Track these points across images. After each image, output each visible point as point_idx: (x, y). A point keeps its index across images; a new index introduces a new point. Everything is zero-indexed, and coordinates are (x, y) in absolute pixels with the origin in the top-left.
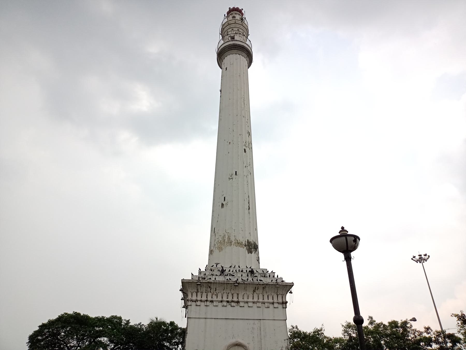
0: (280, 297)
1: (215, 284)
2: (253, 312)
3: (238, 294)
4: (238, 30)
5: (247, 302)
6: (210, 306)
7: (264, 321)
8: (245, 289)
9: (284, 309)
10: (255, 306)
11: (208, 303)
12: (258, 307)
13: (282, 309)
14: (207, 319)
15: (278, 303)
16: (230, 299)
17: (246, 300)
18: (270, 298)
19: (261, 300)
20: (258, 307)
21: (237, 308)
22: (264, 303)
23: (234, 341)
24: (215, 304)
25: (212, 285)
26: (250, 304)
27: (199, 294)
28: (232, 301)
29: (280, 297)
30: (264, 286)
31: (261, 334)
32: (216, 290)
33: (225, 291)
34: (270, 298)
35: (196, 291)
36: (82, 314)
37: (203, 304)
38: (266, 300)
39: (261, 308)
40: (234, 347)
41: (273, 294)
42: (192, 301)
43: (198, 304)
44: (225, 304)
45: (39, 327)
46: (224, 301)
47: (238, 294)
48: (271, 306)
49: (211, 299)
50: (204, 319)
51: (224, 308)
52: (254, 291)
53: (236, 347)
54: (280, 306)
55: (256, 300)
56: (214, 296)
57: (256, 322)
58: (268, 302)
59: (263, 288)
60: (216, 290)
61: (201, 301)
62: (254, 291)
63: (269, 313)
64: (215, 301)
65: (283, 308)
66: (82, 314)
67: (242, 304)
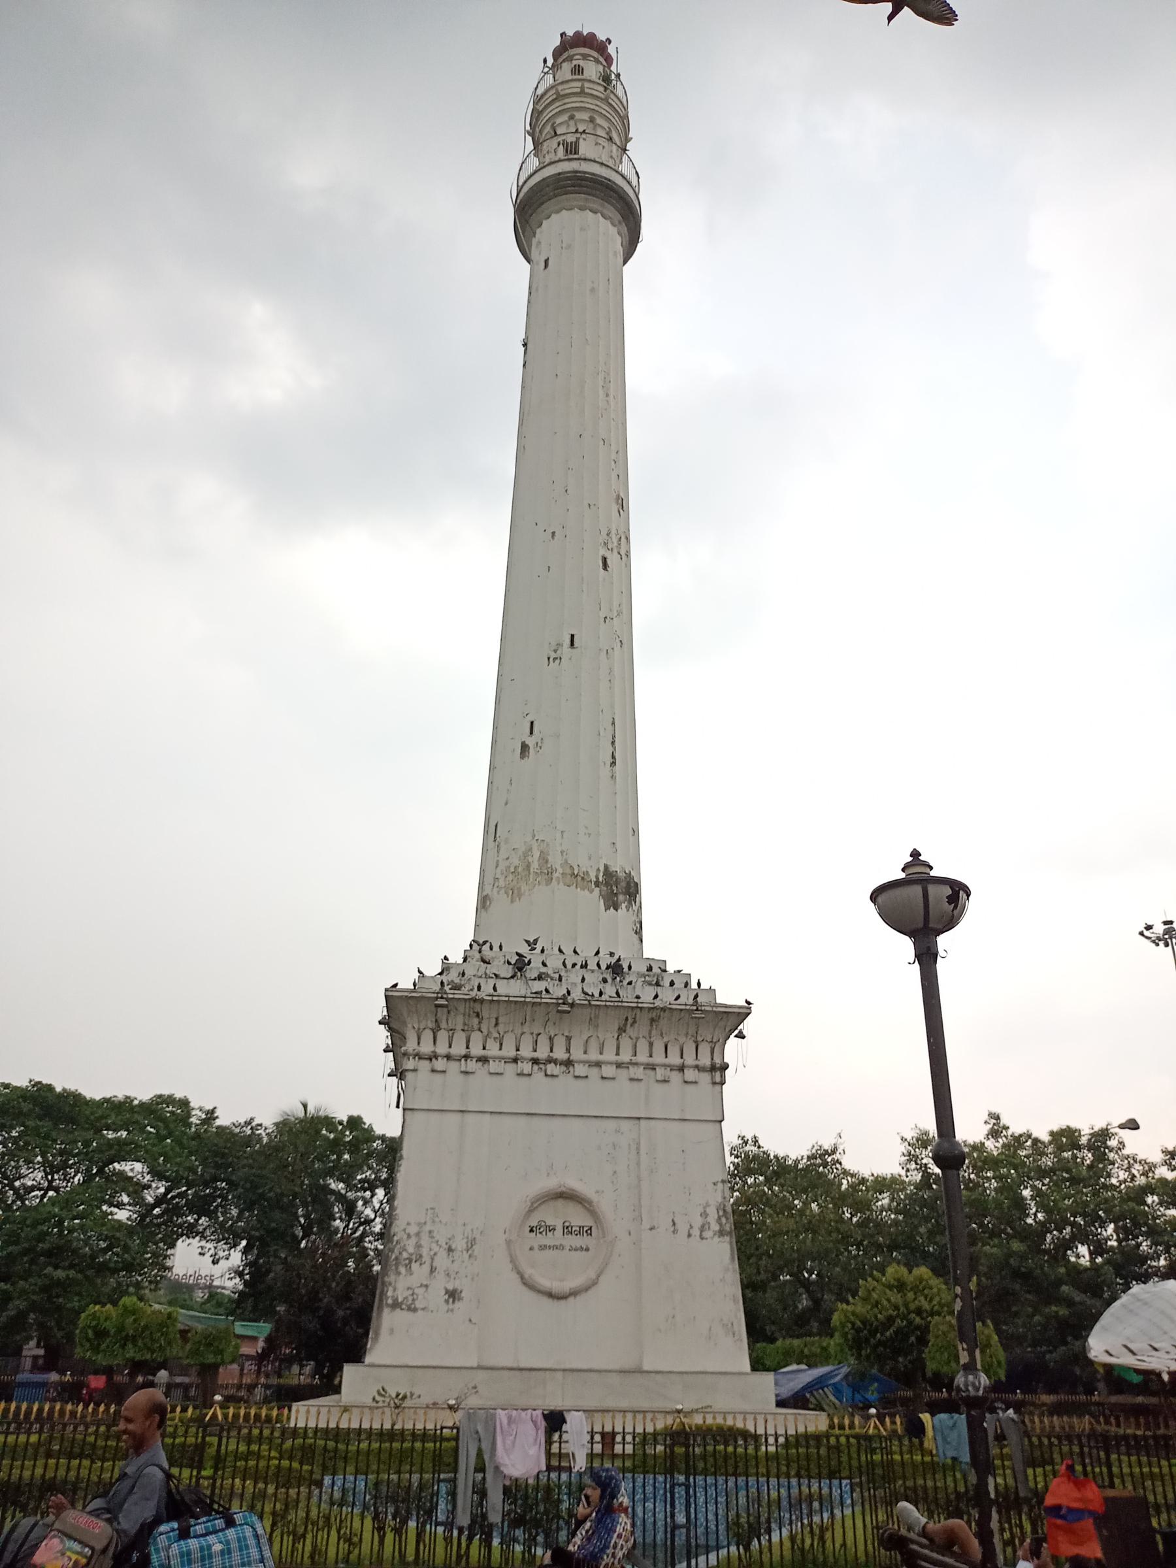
0: (705, 1049)
1: (495, 1006)
2: (621, 1095)
3: (569, 1039)
4: (592, 120)
5: (598, 1064)
8: (593, 1022)
9: (718, 1087)
10: (623, 1074)
11: (472, 1065)
12: (631, 1079)
14: (467, 1116)
16: (542, 1053)
17: (594, 1056)
18: (674, 1052)
20: (631, 1079)
21: (565, 1081)
24: (493, 1066)
25: (486, 1006)
26: (608, 1071)
27: (443, 1036)
32: (497, 1024)
34: (674, 1052)
35: (431, 1025)
36: (58, 1089)
38: (659, 1058)
41: (682, 1039)
42: (419, 1056)
44: (527, 1067)
47: (569, 1039)
48: (675, 1077)
50: (460, 1114)
52: (622, 1030)
53: (560, 1203)
54: (705, 1078)
55: (625, 1057)
57: (625, 1125)
58: (665, 1066)
59: (652, 1020)
61: (448, 1057)
62: (622, 1030)
63: (669, 1097)
65: (714, 1083)
66: (58, 1089)
67: (580, 1070)
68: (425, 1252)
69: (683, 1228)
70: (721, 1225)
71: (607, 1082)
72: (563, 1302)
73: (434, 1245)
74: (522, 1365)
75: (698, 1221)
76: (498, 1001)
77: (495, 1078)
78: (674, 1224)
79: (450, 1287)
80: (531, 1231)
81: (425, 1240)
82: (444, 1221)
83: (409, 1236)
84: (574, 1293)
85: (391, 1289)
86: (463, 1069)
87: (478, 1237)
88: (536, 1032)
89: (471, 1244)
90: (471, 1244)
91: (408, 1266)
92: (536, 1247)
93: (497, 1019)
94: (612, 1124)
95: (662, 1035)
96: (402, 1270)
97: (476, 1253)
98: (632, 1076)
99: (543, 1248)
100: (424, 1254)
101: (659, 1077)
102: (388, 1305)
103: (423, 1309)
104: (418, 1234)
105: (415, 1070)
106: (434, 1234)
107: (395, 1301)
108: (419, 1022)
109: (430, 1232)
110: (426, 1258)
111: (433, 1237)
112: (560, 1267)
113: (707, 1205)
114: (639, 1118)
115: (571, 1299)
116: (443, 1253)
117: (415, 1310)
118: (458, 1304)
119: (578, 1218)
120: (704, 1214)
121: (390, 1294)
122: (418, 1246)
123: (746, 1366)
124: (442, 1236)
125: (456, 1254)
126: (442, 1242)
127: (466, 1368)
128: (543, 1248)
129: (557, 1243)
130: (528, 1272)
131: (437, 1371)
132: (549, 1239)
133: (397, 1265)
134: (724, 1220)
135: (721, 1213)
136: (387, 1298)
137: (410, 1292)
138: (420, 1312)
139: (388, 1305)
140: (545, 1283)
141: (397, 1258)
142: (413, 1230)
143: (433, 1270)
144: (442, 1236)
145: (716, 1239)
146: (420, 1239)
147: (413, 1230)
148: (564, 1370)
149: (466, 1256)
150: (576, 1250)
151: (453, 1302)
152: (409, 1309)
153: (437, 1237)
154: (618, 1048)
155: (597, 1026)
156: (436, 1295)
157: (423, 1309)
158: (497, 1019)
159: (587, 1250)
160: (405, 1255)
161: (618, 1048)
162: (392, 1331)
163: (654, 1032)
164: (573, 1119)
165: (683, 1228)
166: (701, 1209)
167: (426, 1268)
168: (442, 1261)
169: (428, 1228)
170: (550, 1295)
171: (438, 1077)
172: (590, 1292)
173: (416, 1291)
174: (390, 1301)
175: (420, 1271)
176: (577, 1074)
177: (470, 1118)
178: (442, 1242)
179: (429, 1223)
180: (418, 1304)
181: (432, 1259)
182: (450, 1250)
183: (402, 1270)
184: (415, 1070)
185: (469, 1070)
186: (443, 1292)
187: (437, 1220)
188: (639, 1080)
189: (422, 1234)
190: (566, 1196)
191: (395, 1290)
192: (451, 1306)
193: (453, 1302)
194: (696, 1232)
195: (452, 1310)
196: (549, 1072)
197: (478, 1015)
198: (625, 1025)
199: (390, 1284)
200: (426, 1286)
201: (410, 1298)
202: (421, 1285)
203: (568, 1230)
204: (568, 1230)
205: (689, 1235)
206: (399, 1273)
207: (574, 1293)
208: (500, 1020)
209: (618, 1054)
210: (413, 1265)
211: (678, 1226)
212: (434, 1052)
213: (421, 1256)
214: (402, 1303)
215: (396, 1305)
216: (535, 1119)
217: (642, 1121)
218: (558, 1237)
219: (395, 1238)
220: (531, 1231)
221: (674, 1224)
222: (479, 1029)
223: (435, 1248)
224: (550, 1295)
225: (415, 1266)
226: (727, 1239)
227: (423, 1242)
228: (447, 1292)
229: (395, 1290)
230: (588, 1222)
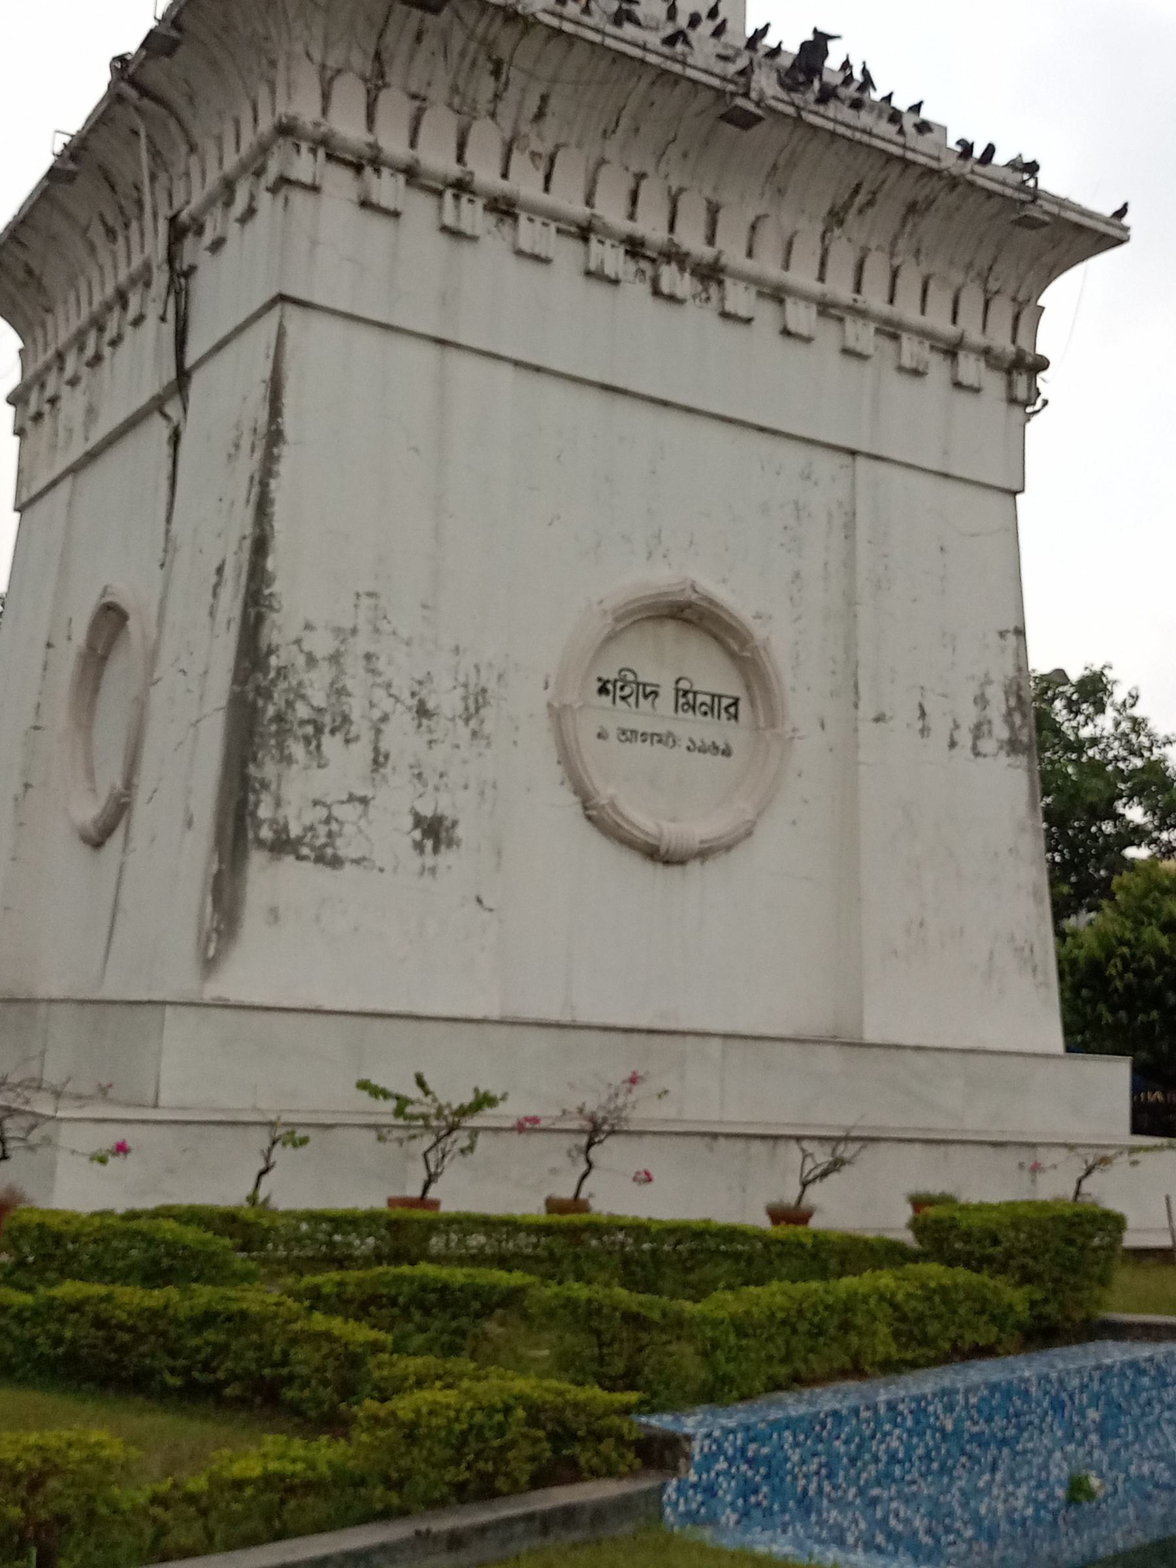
0: (1002, 311)
1: (556, 49)
2: (811, 383)
3: (713, 211)
6: (487, 241)
7: (882, 469)
8: (777, 180)
9: (1017, 412)
10: (828, 335)
12: (847, 352)
13: (1004, 405)
14: (452, 354)
15: (986, 353)
16: (651, 226)
17: (768, 266)
18: (940, 302)
19: (874, 298)
20: (847, 352)
21: (696, 318)
22: (891, 330)
23: (660, 578)
24: (529, 234)
25: (534, 42)
26: (801, 316)
27: (394, 106)
28: (674, 255)
29: (1002, 311)
30: (921, 193)
31: (849, 563)
32: (540, 115)
33: (611, 150)
34: (940, 302)
35: (361, 62)
37: (419, 209)
39: (868, 369)
40: (649, 627)
41: (957, 277)
43: (386, 202)
44: (613, 259)
45: (1042, 309)
46: (607, 233)
47: (713, 211)
49: (501, 186)
50: (432, 350)
51: (599, 291)
52: (836, 217)
53: (670, 629)
54: (994, 383)
55: (840, 288)
56: (519, 160)
57: (826, 464)
58: (924, 334)
59: (912, 208)
60: (540, 115)
61: (411, 174)
62: (836, 217)
63: (919, 413)
64: (535, 211)
65: (1012, 400)
67: (739, 298)
68: (356, 707)
69: (940, 728)
70: (1012, 726)
71: (790, 342)
72: (675, 871)
73: (379, 694)
74: (582, 1019)
75: (969, 715)
76: (572, 38)
77: (529, 267)
78: (923, 714)
79: (427, 811)
80: (603, 690)
81: (355, 679)
82: (405, 633)
83: (311, 660)
84: (704, 854)
85: (266, 799)
86: (449, 219)
87: (492, 686)
88: (635, 168)
89: (476, 703)
90: (476, 703)
91: (313, 742)
92: (613, 734)
93: (544, 99)
94: (794, 455)
95: (918, 252)
96: (297, 750)
97: (488, 728)
98: (851, 343)
99: (628, 735)
100: (355, 716)
101: (907, 362)
102: (261, 843)
103: (357, 862)
104: (335, 658)
105: (314, 189)
106: (381, 665)
107: (281, 830)
108: (327, 44)
109: (368, 657)
110: (360, 726)
111: (373, 672)
112: (666, 792)
113: (988, 682)
114: (853, 453)
115: (694, 867)
116: (403, 719)
117: (336, 862)
118: (447, 857)
119: (712, 674)
120: (981, 701)
121: (264, 812)
122: (339, 692)
123: (1055, 1041)
124: (400, 671)
125: (439, 725)
126: (402, 687)
127: (639, 1031)
128: (628, 735)
129: (661, 729)
130: (605, 791)
131: (657, 1039)
132: (640, 717)
133: (282, 734)
134: (1017, 719)
135: (1013, 702)
136: (258, 824)
137: (322, 812)
138: (348, 868)
139: (261, 843)
140: (644, 819)
141: (279, 718)
142: (321, 644)
143: (379, 760)
144: (400, 671)
145: (1003, 759)
146: (341, 672)
147: (321, 644)
148: (726, 1036)
149: (464, 732)
150: (703, 750)
151: (436, 850)
152: (320, 859)
153: (389, 673)
154: (823, 264)
155: (781, 192)
156: (386, 831)
157: (357, 862)
158: (544, 99)
159: (727, 752)
160: (302, 711)
161: (823, 264)
162: (274, 914)
163: (902, 244)
164: (716, 425)
165: (940, 728)
166: (973, 689)
167: (362, 751)
168: (401, 736)
169: (362, 644)
170: (655, 854)
171: (379, 226)
172: (734, 853)
173: (338, 811)
174: (266, 833)
175: (344, 763)
176: (729, 307)
177: (464, 367)
178: (402, 687)
179: (364, 629)
180: (344, 848)
181: (378, 731)
182: (423, 711)
183: (297, 750)
184: (314, 189)
185: (466, 226)
186: (409, 821)
187: (385, 626)
188: (861, 357)
189: (348, 662)
190: (689, 614)
191: (278, 803)
192: (429, 860)
193: (436, 850)
194: (965, 738)
195: (433, 870)
196: (665, 288)
197: (496, 73)
198: (846, 207)
199: (265, 785)
200: (364, 801)
201: (322, 830)
202: (351, 798)
203: (686, 699)
204: (686, 699)
205: (953, 744)
206: (288, 760)
207: (704, 854)
208: (553, 103)
209: (821, 278)
210: (326, 739)
211: (932, 720)
212: (373, 146)
213: (346, 719)
214: (300, 840)
215: (282, 845)
216: (623, 406)
217: (861, 462)
218: (661, 715)
219: (273, 661)
220: (603, 690)
221: (923, 714)
222: (493, 115)
223: (387, 704)
224: (655, 854)
225: (331, 744)
226: (1022, 760)
227: (350, 684)
228: (418, 821)
229: (278, 803)
230: (728, 684)
